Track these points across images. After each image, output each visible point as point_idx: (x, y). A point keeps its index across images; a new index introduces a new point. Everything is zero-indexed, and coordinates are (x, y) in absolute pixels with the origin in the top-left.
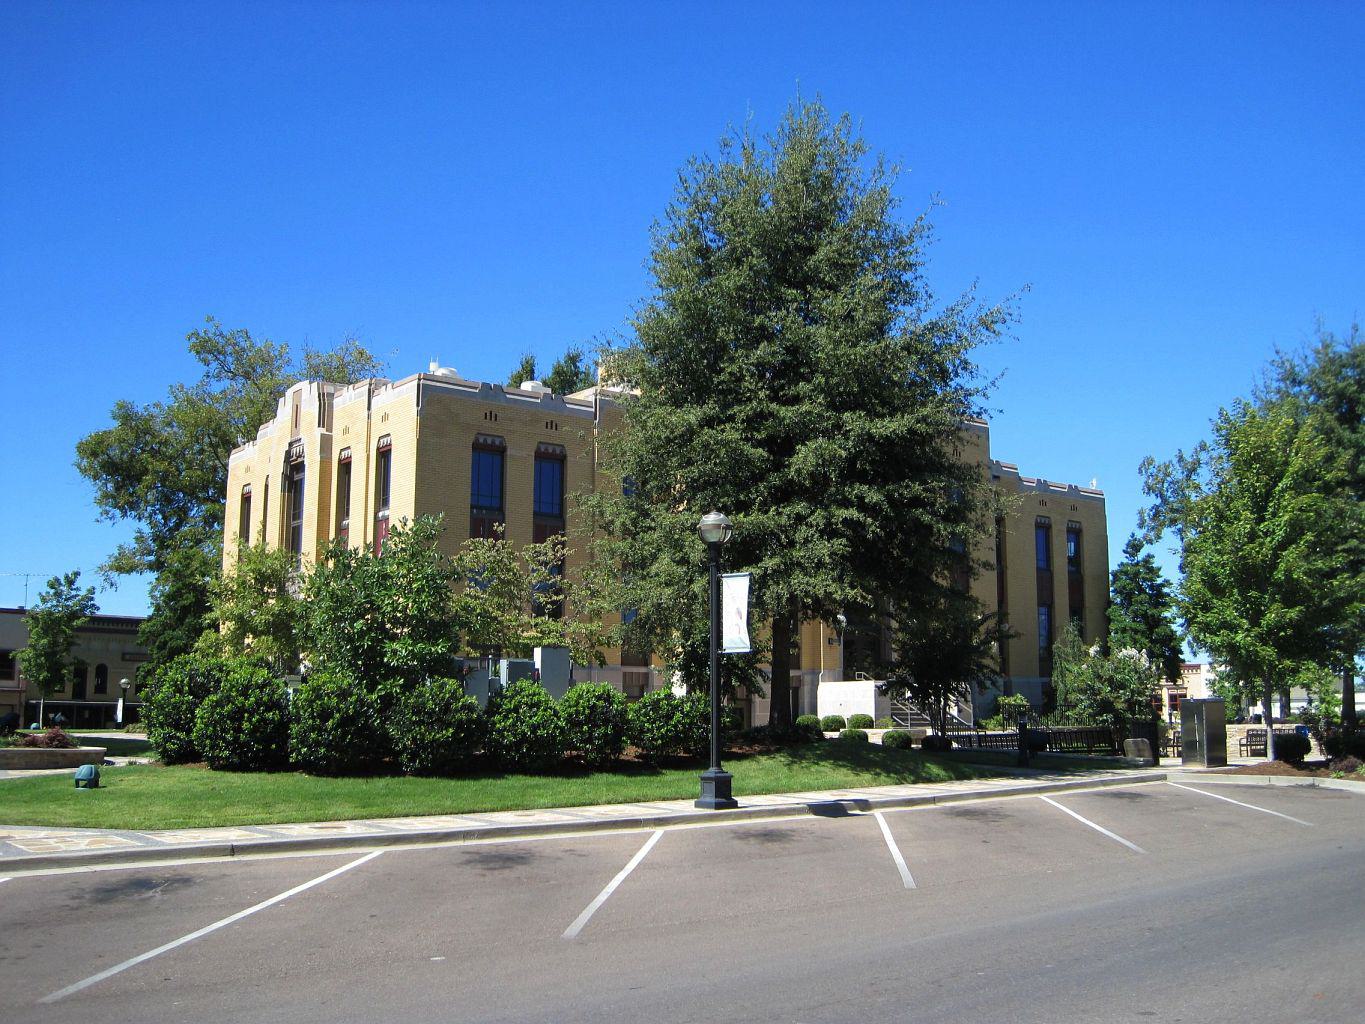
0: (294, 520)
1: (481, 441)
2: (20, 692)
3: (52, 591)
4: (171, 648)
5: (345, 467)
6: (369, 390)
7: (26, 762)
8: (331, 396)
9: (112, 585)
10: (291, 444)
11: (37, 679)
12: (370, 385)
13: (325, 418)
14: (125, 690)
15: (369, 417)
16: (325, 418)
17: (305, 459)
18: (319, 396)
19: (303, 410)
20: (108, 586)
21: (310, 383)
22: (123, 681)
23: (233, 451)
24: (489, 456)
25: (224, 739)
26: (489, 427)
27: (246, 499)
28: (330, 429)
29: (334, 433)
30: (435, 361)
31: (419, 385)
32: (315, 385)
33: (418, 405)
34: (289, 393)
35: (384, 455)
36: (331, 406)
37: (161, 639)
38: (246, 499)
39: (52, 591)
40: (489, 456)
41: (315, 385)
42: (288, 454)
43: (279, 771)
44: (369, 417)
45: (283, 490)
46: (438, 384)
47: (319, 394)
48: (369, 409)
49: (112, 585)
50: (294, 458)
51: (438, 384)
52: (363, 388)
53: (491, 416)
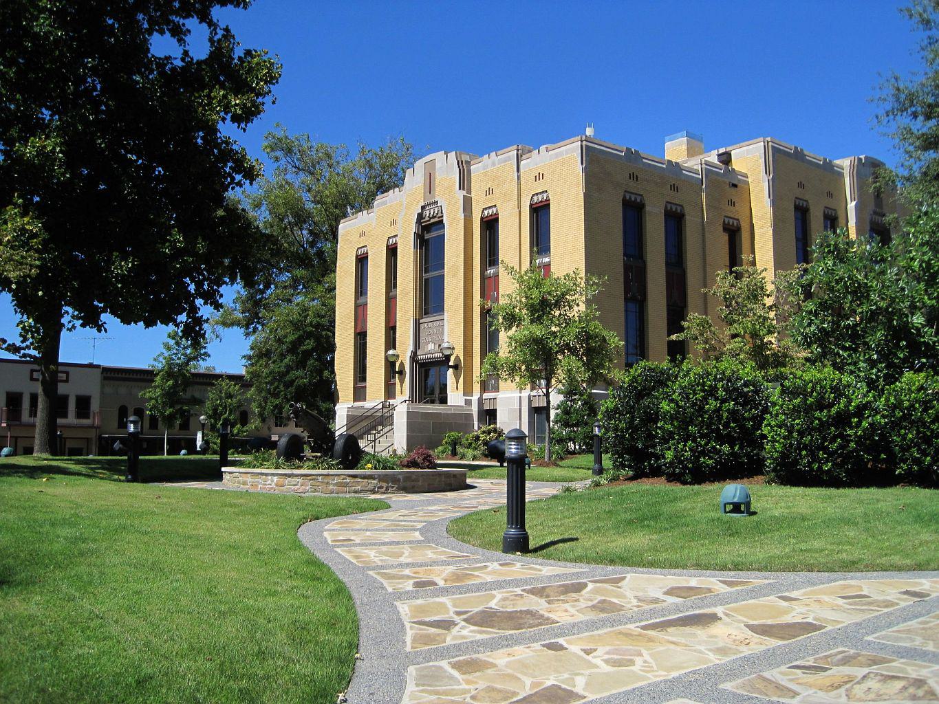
1: (628, 197)
2: (97, 428)
3: (174, 341)
4: (299, 386)
5: (490, 225)
6: (517, 154)
7: (429, 485)
8: (468, 163)
9: (217, 337)
10: (423, 208)
11: (162, 414)
12: (518, 150)
13: (465, 181)
14: (203, 425)
16: (465, 181)
17: (444, 218)
18: (458, 164)
19: (438, 177)
20: (214, 337)
21: (446, 153)
22: (202, 417)
23: (342, 221)
24: (633, 211)
25: (825, 449)
26: (633, 186)
27: (362, 261)
28: (469, 192)
29: (472, 195)
31: (581, 146)
32: (452, 155)
33: (582, 163)
34: (419, 164)
35: (392, 251)
36: (469, 171)
37: (288, 378)
39: (174, 341)
40: (633, 211)
41: (452, 155)
42: (420, 216)
43: (822, 487)
46: (596, 146)
48: (518, 171)
49: (217, 337)
50: (427, 219)
51: (596, 146)
53: (634, 177)
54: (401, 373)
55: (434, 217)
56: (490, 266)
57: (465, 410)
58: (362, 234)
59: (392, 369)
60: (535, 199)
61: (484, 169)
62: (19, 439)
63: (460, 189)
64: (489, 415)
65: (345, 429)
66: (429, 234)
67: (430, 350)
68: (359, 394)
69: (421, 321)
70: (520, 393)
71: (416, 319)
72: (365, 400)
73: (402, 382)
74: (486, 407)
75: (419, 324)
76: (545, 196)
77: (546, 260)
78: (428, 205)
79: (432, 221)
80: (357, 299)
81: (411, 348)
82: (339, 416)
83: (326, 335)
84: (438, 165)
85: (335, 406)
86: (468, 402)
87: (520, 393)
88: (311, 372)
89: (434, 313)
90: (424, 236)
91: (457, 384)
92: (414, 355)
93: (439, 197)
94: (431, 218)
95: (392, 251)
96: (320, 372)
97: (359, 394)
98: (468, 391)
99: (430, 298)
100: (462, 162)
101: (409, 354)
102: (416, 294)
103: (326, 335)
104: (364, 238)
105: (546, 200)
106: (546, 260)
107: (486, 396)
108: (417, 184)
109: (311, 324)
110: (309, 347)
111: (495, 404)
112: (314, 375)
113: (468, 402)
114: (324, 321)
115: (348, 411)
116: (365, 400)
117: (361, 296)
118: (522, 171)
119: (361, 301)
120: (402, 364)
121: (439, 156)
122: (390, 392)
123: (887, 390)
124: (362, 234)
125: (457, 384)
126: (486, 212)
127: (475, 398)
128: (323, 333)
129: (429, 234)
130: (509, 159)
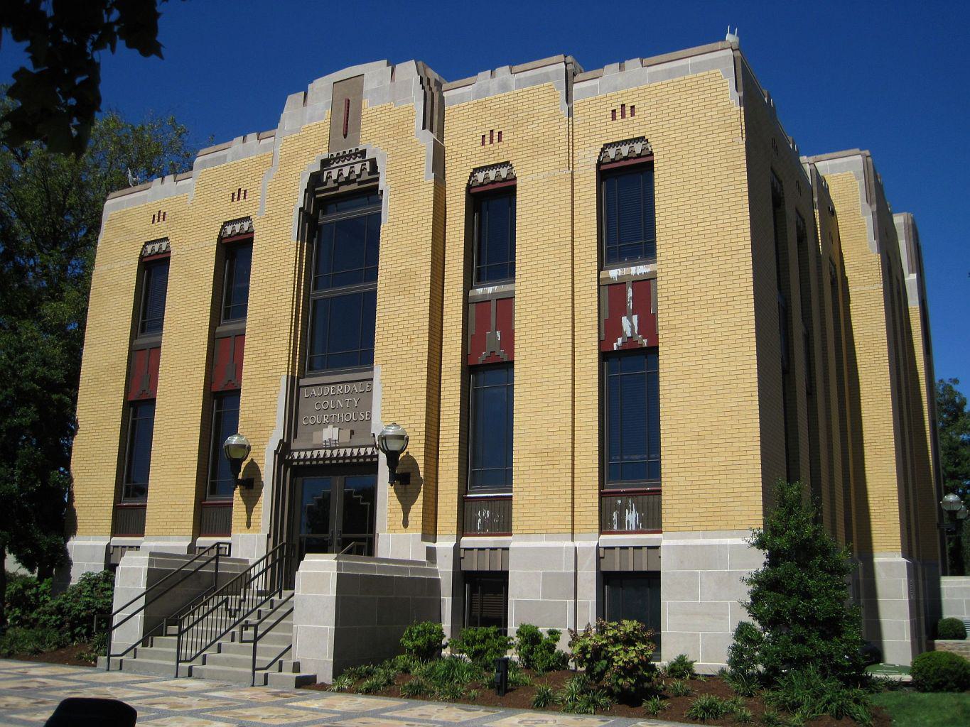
0: (316, 288)
10: (325, 163)
13: (433, 117)
15: (570, 113)
16: (433, 117)
18: (421, 82)
27: (154, 269)
30: (732, 32)
34: (322, 87)
36: (442, 99)
38: (154, 269)
42: (315, 179)
44: (570, 113)
45: (301, 236)
47: (421, 79)
50: (331, 184)
52: (555, 67)
54: (251, 485)
55: (348, 181)
56: (479, 280)
57: (424, 571)
58: (239, 194)
59: (221, 472)
60: (229, 229)
61: (478, 97)
62: (106, 668)
63: (424, 128)
64: (484, 589)
65: (141, 602)
66: (341, 221)
67: (328, 437)
68: (129, 515)
69: (302, 382)
70: (573, 540)
71: (293, 377)
72: (140, 532)
73: (251, 503)
74: (470, 565)
75: (299, 387)
76: (246, 225)
77: (640, 270)
78: (339, 158)
79: (343, 189)
80: (215, 321)
81: (277, 434)
82: (126, 571)
83: (60, 400)
84: (369, 85)
85: (67, 540)
86: (431, 554)
87: (573, 540)
88: (26, 471)
89: (323, 368)
90: (317, 220)
91: (406, 512)
92: (284, 451)
93: (371, 139)
94: (341, 184)
95: (234, 252)
96: (817, 513)
97: (129, 515)
98: (430, 532)
99: (337, 332)
100: (429, 80)
101: (273, 445)
102: (296, 327)
103: (60, 400)
104: (162, 224)
105: (247, 233)
106: (640, 270)
107: (467, 541)
108: (311, 120)
109: (32, 377)
110: (26, 421)
111: (505, 560)
112: (33, 476)
113: (431, 554)
114: (58, 376)
115: (150, 562)
116: (140, 532)
117: (143, 331)
118: (576, 101)
119: (227, 328)
120: (253, 467)
121: (374, 73)
122: (210, 516)
123: (36, 481)
124: (160, 217)
125: (406, 512)
126: (149, 248)
127: (445, 545)
128: (55, 397)
129: (341, 221)
130: (546, 78)
